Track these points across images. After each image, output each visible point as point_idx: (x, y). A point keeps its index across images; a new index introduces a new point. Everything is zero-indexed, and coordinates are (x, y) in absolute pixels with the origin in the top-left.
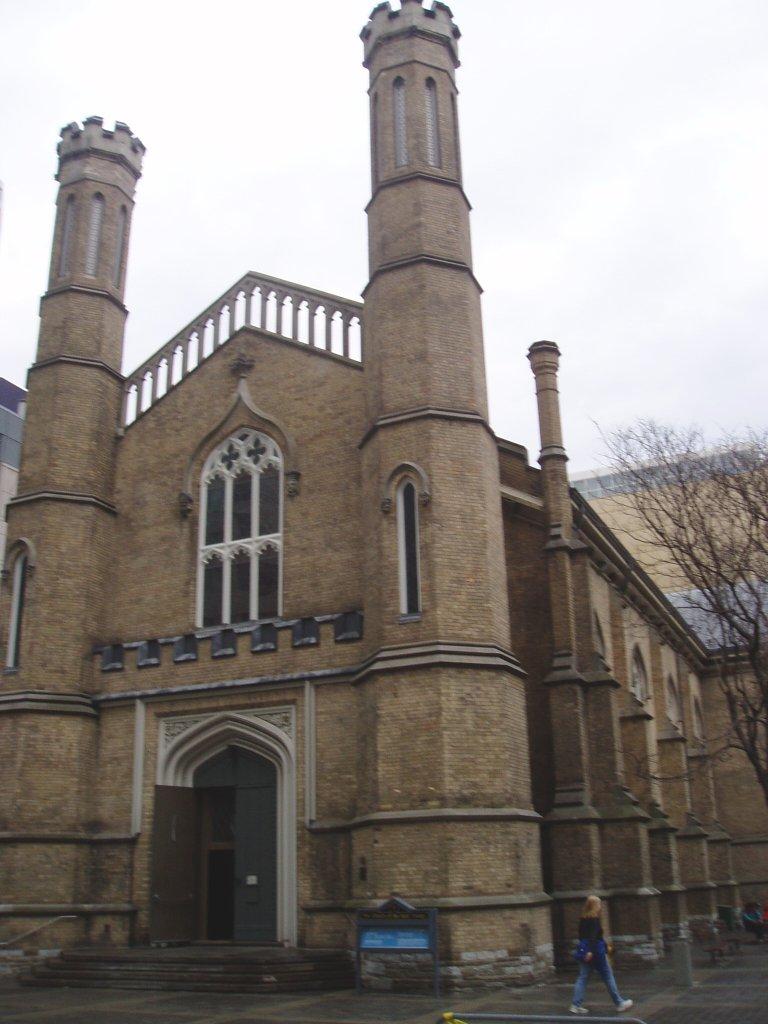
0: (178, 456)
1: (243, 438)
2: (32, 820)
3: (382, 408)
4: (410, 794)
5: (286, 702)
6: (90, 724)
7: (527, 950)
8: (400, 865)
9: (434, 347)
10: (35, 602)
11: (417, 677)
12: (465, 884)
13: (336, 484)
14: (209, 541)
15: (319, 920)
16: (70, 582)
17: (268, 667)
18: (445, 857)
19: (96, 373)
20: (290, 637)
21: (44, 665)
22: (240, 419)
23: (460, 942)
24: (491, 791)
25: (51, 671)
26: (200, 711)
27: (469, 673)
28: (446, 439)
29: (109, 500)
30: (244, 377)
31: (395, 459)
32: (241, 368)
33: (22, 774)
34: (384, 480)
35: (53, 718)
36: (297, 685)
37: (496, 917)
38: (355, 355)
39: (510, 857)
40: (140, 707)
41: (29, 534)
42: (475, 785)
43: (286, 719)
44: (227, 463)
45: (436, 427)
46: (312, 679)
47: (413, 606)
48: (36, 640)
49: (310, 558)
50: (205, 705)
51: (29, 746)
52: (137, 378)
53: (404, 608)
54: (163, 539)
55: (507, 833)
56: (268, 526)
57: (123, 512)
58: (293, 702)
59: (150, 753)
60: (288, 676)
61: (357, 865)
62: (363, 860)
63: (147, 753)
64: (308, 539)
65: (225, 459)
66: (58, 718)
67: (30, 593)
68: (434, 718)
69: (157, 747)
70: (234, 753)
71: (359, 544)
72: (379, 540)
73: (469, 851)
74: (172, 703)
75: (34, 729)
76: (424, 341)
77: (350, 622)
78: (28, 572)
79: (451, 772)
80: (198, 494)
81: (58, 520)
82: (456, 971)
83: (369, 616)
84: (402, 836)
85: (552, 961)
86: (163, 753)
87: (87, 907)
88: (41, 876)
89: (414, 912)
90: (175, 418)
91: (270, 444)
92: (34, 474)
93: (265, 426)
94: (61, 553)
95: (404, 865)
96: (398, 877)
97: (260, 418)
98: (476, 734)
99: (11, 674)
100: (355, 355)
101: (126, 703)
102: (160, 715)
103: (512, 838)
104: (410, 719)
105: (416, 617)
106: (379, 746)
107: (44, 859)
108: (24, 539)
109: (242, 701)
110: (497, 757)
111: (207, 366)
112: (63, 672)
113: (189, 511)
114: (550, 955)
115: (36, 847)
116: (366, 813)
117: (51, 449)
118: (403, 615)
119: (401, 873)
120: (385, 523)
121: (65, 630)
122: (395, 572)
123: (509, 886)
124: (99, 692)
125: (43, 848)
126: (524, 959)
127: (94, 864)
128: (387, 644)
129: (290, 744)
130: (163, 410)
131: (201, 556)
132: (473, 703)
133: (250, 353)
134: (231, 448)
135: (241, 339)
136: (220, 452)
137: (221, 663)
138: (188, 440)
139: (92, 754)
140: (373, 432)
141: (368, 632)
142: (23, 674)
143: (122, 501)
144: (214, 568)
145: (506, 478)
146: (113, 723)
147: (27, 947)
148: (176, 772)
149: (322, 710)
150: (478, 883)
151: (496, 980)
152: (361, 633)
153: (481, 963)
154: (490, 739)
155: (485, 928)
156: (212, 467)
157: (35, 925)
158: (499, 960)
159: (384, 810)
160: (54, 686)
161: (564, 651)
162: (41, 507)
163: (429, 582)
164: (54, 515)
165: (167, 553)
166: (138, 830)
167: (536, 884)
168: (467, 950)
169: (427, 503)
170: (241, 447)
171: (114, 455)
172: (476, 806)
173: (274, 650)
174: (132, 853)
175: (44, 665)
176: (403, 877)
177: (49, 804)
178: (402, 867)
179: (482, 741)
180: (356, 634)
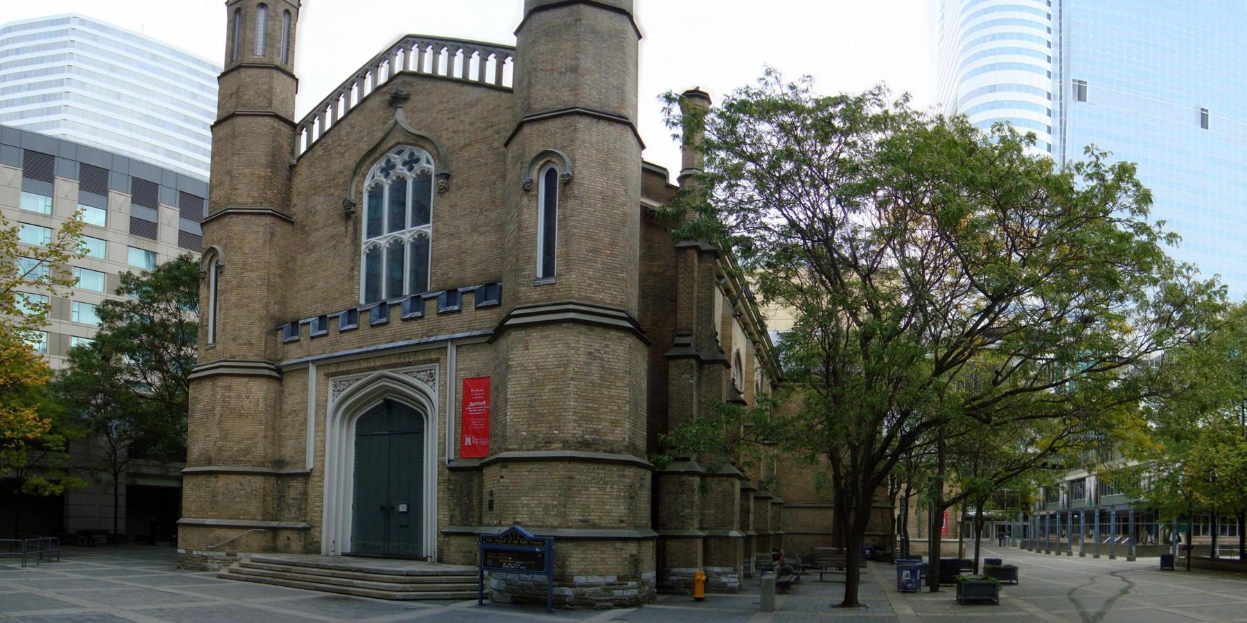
1: (399, 153)
2: (230, 458)
3: (529, 108)
4: (535, 437)
5: (431, 361)
6: (275, 385)
7: (636, 576)
8: (523, 498)
9: (586, 63)
10: (224, 292)
11: (549, 332)
12: (581, 518)
13: (483, 181)
14: (370, 235)
15: (454, 541)
16: (253, 275)
17: (415, 333)
18: (567, 492)
19: (268, 120)
20: (435, 306)
21: (234, 340)
22: (398, 137)
23: (572, 567)
24: (611, 438)
25: (240, 344)
26: (360, 371)
27: (597, 330)
28: (592, 134)
29: (285, 212)
30: (401, 107)
31: (537, 146)
32: (397, 100)
33: (220, 422)
34: (526, 165)
35: (243, 380)
36: (441, 346)
37: (608, 548)
38: (508, 82)
39: (624, 497)
40: (312, 370)
41: (219, 242)
42: (597, 431)
43: (431, 375)
44: (384, 173)
45: (582, 123)
46: (452, 340)
47: (548, 270)
48: (228, 321)
49: (457, 242)
50: (364, 365)
51: (225, 402)
52: (307, 122)
53: (540, 274)
54: (332, 237)
55: (623, 476)
56: (422, 215)
57: (299, 221)
58: (437, 360)
59: (322, 406)
60: (433, 339)
61: (486, 498)
62: (491, 494)
63: (318, 405)
64: (455, 227)
65: (383, 170)
66: (247, 380)
67: (221, 286)
68: (562, 369)
69: (326, 401)
70: (388, 404)
71: (500, 227)
72: (520, 214)
73: (587, 489)
74: (338, 364)
75: (229, 388)
76: (577, 59)
77: (490, 291)
78: (219, 269)
79: (575, 390)
80: (361, 199)
81: (241, 228)
82: (568, 591)
83: (507, 286)
84: (526, 474)
85: (654, 585)
86: (331, 406)
87: (275, 524)
88: (237, 499)
89: (533, 540)
91: (424, 155)
92: (221, 198)
93: (420, 140)
94: (245, 253)
95: (528, 498)
96: (520, 509)
97: (414, 134)
98: (601, 386)
99: (211, 348)
100: (508, 82)
101: (302, 368)
102: (328, 375)
103: (626, 480)
104: (539, 369)
105: (552, 281)
106: (509, 393)
107: (239, 487)
108: (216, 246)
109: (393, 361)
110: (620, 408)
111: (367, 103)
112: (251, 344)
113: (353, 212)
114: (653, 581)
115: (232, 477)
116: (496, 453)
117: (232, 178)
118: (539, 279)
119: (524, 505)
120: (525, 200)
121: (250, 312)
122: (535, 240)
123: (621, 521)
124: (280, 360)
125: (239, 478)
126: (630, 584)
127: (279, 492)
128: (519, 304)
129: (435, 396)
130: (329, 140)
131: (363, 247)
132: (601, 359)
133: (404, 91)
134: (389, 161)
135: (398, 81)
136: (378, 166)
137: (378, 330)
138: (351, 160)
139: (276, 406)
140: (520, 126)
141: (506, 296)
142: (219, 347)
143: (298, 208)
144: (374, 254)
145: (646, 192)
146: (292, 384)
147: (228, 549)
148: (341, 426)
149: (462, 367)
150: (593, 517)
151: (607, 601)
152: (500, 301)
153: (592, 585)
154: (614, 392)
155: (596, 556)
156: (373, 177)
157: (233, 535)
158: (609, 584)
159: (510, 450)
160: (244, 355)
161: (688, 332)
162: (226, 220)
164: (237, 225)
165: (334, 247)
166: (311, 467)
167: (645, 522)
168: (579, 574)
169: (568, 181)
170: (397, 160)
171: (290, 179)
172: (597, 450)
173: (422, 317)
174: (306, 483)
175: (234, 340)
176: (525, 509)
177: (243, 447)
178: (525, 500)
179: (606, 393)
180: (495, 302)
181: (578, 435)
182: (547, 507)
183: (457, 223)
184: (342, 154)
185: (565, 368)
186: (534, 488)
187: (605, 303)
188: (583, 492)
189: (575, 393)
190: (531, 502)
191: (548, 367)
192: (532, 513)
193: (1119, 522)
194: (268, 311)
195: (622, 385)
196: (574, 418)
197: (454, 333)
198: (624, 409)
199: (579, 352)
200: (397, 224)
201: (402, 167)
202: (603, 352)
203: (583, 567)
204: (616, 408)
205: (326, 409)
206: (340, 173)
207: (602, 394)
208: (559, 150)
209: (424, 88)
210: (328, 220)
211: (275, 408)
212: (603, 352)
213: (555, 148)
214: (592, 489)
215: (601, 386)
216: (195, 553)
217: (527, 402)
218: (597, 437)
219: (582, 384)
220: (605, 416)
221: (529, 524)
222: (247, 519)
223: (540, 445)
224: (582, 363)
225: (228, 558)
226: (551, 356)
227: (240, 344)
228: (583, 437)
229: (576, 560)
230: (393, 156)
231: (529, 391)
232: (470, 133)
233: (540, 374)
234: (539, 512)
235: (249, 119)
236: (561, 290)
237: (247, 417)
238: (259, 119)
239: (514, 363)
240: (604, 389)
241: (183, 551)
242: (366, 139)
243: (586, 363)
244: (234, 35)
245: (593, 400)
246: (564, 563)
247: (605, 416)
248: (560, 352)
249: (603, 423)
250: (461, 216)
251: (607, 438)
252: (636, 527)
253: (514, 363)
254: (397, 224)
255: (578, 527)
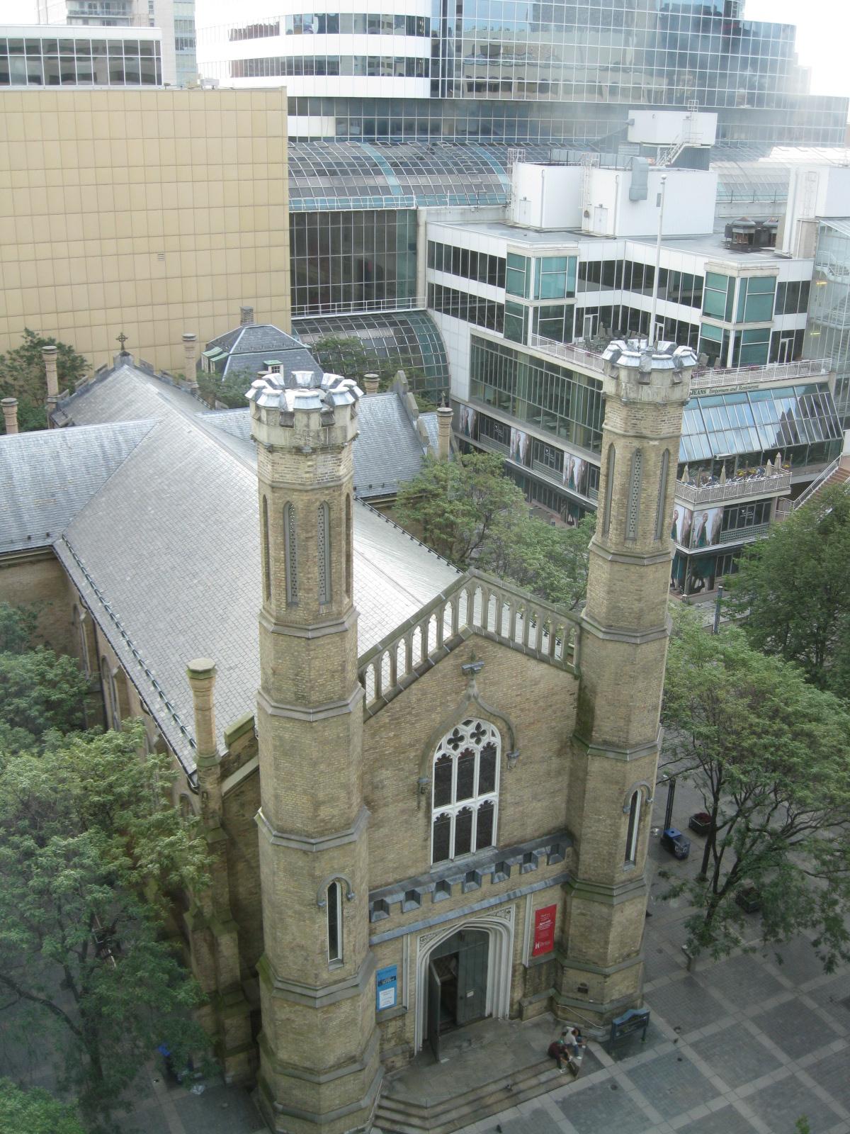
0: (414, 745)
49: (521, 808)
54: (403, 812)
56: (487, 786)
90: (410, 713)
134: (456, 732)
163: (761, 880)
165: (406, 822)
193: (317, 308)
230: (461, 727)
244: (292, 565)
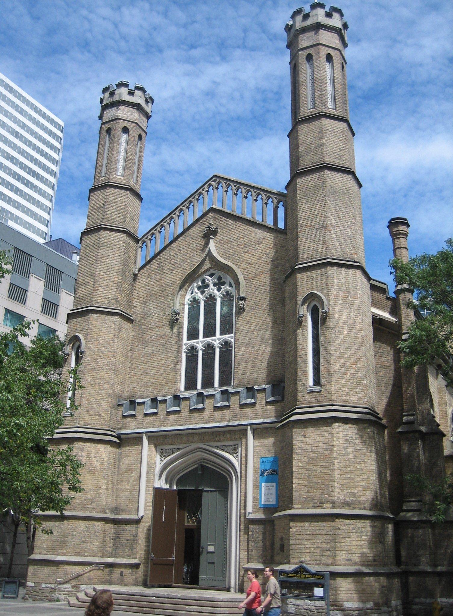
1: (211, 275)
2: (79, 505)
8: (305, 543)
9: (331, 220)
16: (105, 361)
19: (123, 235)
21: (88, 411)
24: (364, 499)
25: (92, 415)
29: (128, 312)
41: (81, 331)
42: (354, 495)
45: (332, 270)
47: (317, 381)
49: (252, 350)
53: (311, 382)
56: (227, 328)
68: (329, 452)
70: (203, 467)
80: (184, 309)
81: (99, 323)
86: (158, 467)
95: (309, 543)
98: (355, 462)
104: (314, 452)
110: (368, 477)
112: (100, 415)
113: (177, 320)
119: (306, 549)
121: (101, 390)
129: (237, 464)
154: (363, 466)
157: (79, 570)
172: (355, 508)
175: (88, 411)
178: (307, 544)
179: (358, 467)
181: (341, 498)
182: (322, 550)
183: (252, 335)
184: (171, 270)
185: (331, 451)
186: (313, 536)
187: (354, 403)
188: (347, 539)
189: (338, 468)
190: (311, 546)
191: (319, 450)
192: (312, 554)
194: (113, 390)
195: (369, 461)
196: (338, 486)
197: (251, 419)
198: (372, 478)
199: (339, 440)
200: (210, 331)
201: (213, 288)
202: (355, 438)
203: (349, 595)
204: (365, 477)
205: (154, 470)
206: (170, 286)
207: (355, 468)
208: (319, 292)
209: (227, 224)
210: (159, 322)
211: (114, 466)
212: (355, 438)
213: (317, 290)
214: (353, 537)
215: (355, 462)
216: (43, 586)
217: (307, 475)
218: (354, 499)
219: (342, 461)
220: (358, 484)
221: (310, 562)
222: (90, 556)
223: (316, 505)
224: (341, 447)
225: (73, 590)
226: (321, 443)
227: (92, 415)
228: (345, 499)
229: (344, 589)
231: (308, 467)
232: (259, 266)
233: (314, 455)
234: (317, 554)
235: (110, 233)
236: (326, 395)
237: (94, 473)
238: (117, 234)
239: (297, 447)
240: (357, 465)
241: (32, 584)
242: (188, 261)
243: (344, 447)
245: (351, 473)
246: (336, 593)
247: (358, 484)
248: (327, 440)
249: (357, 489)
250: (254, 330)
251: (361, 499)
252: (385, 565)
253: (297, 447)
254: (210, 331)
255: (345, 565)
